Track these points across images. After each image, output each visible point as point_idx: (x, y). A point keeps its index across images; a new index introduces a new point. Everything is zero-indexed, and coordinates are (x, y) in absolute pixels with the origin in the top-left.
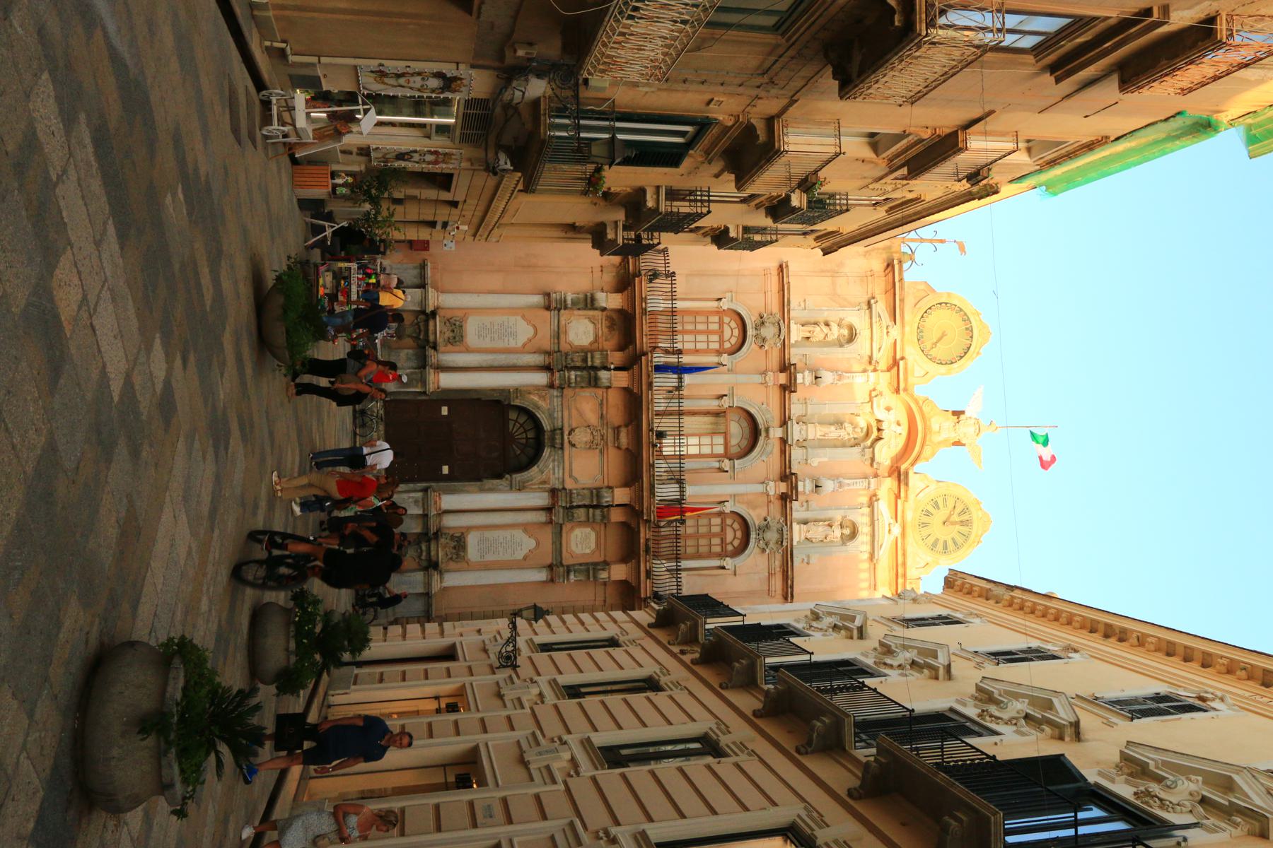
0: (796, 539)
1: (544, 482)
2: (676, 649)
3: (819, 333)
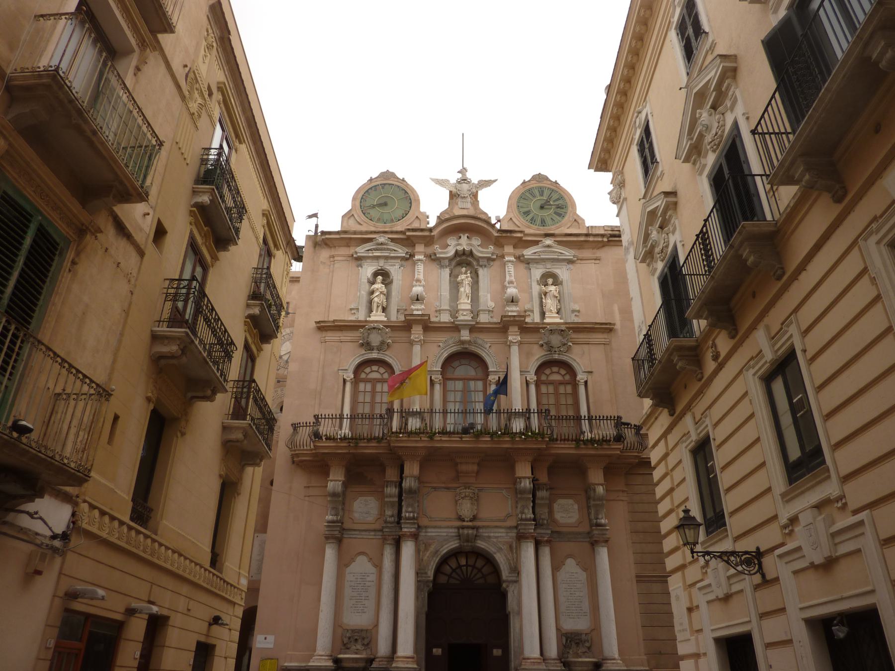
0: (558, 320)
1: (511, 547)
2: (710, 366)
3: (377, 299)
